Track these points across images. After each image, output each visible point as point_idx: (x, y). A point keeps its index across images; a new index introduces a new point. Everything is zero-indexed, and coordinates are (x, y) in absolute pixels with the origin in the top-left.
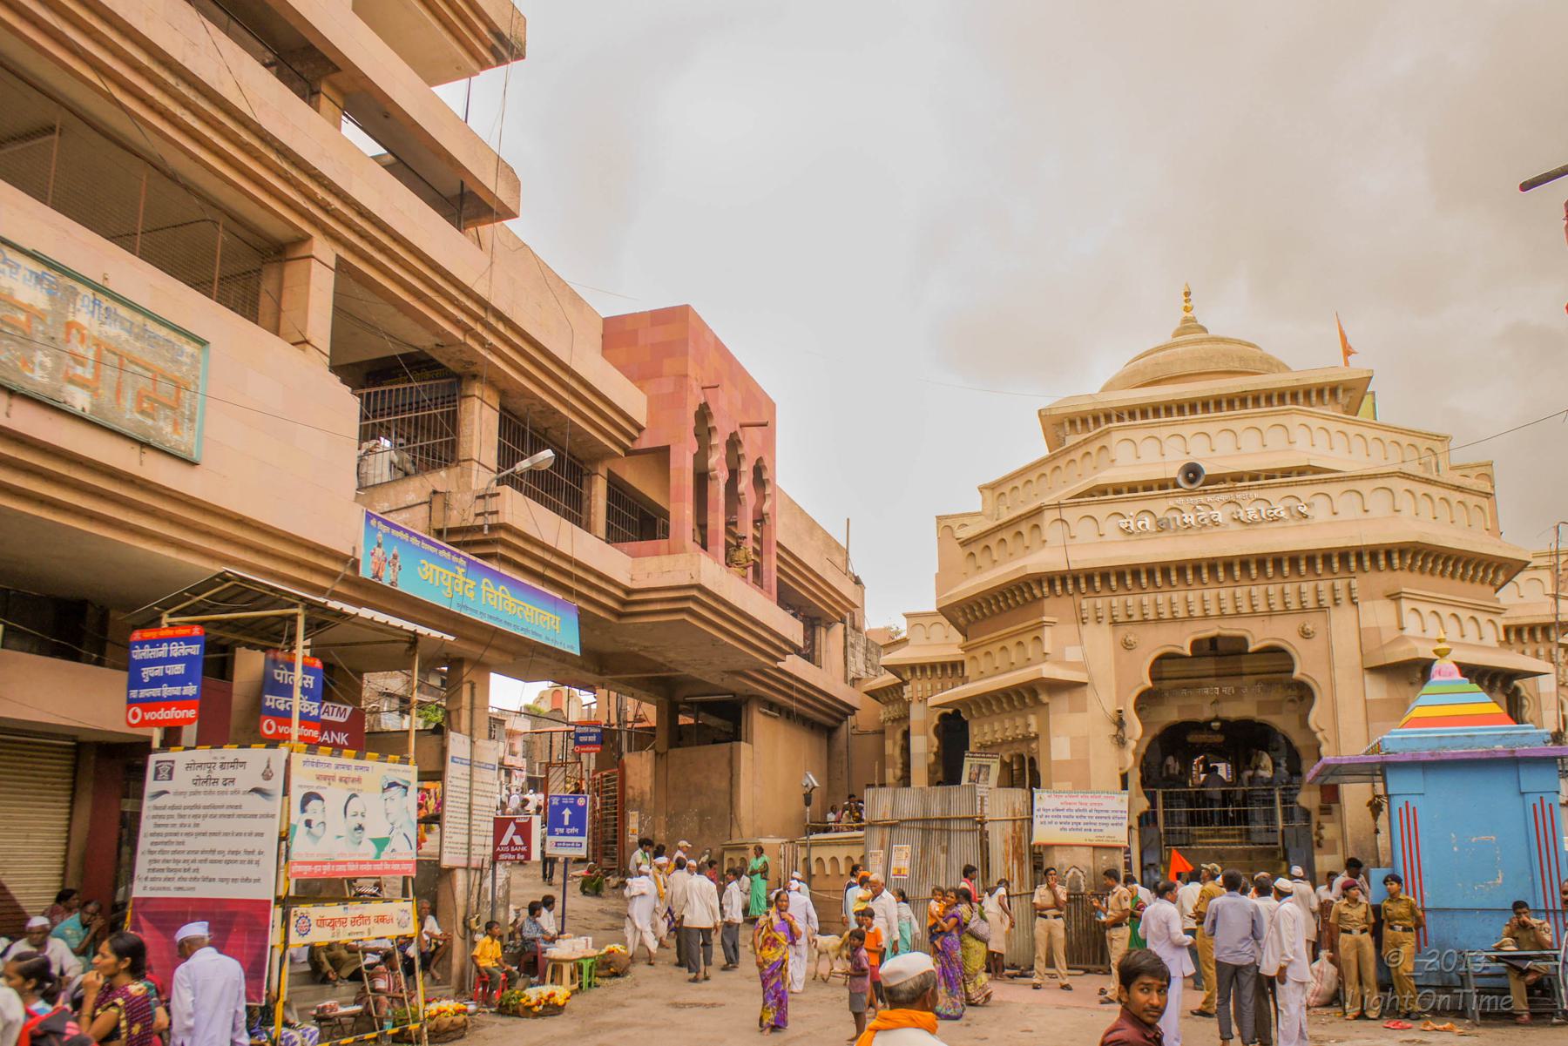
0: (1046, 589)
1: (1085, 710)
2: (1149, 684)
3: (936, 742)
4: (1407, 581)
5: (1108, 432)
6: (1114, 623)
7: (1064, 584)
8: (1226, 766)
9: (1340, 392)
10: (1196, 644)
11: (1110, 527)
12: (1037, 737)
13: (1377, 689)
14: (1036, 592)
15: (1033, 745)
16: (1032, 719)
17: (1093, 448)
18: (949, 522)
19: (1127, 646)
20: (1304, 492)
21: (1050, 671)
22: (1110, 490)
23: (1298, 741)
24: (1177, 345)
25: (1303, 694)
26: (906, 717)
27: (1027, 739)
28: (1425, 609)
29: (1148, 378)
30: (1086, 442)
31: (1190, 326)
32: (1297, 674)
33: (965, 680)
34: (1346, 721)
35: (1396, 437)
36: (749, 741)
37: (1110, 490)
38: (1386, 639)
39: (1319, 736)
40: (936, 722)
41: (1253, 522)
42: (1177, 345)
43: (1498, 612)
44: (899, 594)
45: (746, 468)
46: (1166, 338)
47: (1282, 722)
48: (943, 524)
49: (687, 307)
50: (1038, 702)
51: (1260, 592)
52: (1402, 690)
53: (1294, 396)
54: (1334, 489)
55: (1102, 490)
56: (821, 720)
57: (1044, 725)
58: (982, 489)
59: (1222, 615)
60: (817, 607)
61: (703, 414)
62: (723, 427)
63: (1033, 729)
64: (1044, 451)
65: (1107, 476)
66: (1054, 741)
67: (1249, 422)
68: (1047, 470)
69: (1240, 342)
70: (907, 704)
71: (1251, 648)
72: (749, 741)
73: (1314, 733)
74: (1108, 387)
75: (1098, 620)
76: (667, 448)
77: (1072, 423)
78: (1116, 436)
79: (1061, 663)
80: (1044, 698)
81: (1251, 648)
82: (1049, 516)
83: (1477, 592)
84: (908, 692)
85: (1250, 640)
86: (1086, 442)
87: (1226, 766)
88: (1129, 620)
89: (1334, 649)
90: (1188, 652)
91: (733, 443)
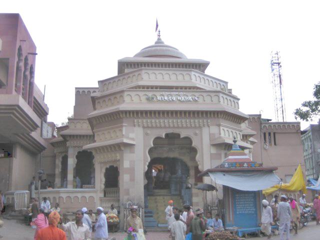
0: (124, 115)
1: (134, 153)
2: (153, 146)
3: (76, 160)
4: (223, 123)
5: (141, 70)
6: (144, 127)
7: (130, 114)
8: (171, 169)
9: (201, 66)
10: (167, 135)
11: (143, 98)
12: (119, 160)
13: (213, 151)
14: (121, 116)
15: (118, 163)
16: (118, 155)
17: (136, 74)
18: (79, 90)
19: (147, 134)
20: (197, 94)
21: (126, 141)
22: (146, 87)
23: (190, 164)
24: (156, 46)
25: (194, 151)
26: (67, 152)
27: (116, 161)
28: (226, 129)
29: (147, 55)
30: (134, 72)
31: (159, 41)
32: (193, 145)
33: (95, 141)
34: (206, 159)
35: (213, 80)
36: (16, 158)
37: (146, 87)
38: (216, 137)
39: (198, 163)
40: (76, 154)
41: (183, 101)
42: (156, 46)
43: (241, 131)
44: (60, 111)
45: (29, 67)
46: (153, 44)
47: (186, 159)
48: (77, 90)
49: (18, 14)
50: (120, 150)
51: (184, 122)
52: (223, 153)
53: (189, 66)
54: (205, 94)
55: (139, 87)
56: (34, 150)
57: (122, 157)
58: (99, 82)
59: (174, 127)
60: (42, 112)
61: (20, 49)
62: (24, 53)
63: (118, 158)
64: (115, 74)
65: (141, 83)
66: (125, 162)
67: (181, 72)
68: (117, 80)
69: (174, 48)
70: (68, 147)
71: (182, 137)
72: (16, 158)
73: (197, 162)
74: (136, 56)
75: (139, 126)
76: (8, 59)
77: (127, 65)
78: (143, 72)
79: (128, 138)
80: (122, 148)
81: (182, 137)
82: (126, 93)
83: (234, 126)
84: (68, 144)
85: (181, 135)
86: (134, 72)
87: (171, 169)
88: (148, 127)
89: (205, 138)
90: (164, 137)
91: (26, 59)
